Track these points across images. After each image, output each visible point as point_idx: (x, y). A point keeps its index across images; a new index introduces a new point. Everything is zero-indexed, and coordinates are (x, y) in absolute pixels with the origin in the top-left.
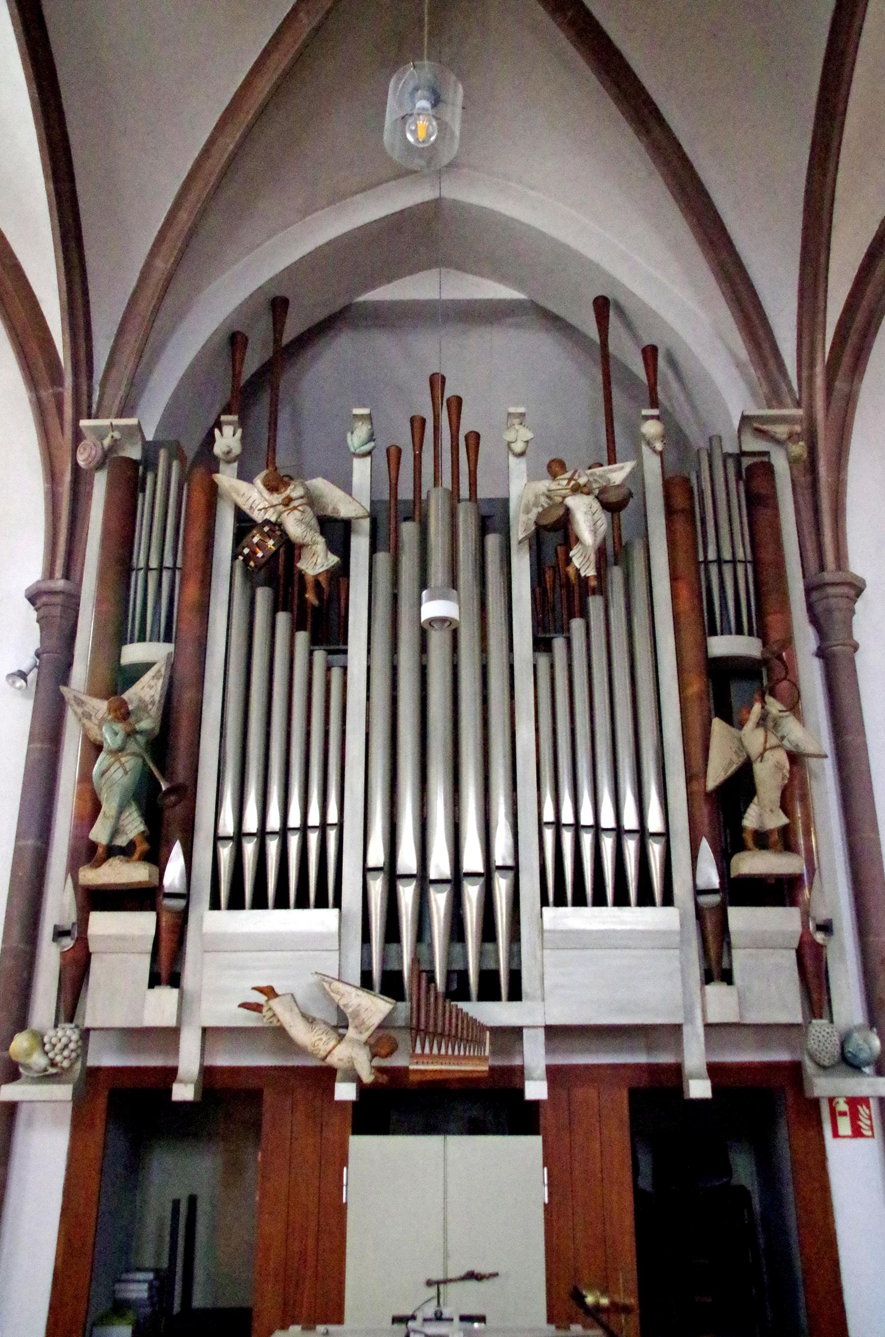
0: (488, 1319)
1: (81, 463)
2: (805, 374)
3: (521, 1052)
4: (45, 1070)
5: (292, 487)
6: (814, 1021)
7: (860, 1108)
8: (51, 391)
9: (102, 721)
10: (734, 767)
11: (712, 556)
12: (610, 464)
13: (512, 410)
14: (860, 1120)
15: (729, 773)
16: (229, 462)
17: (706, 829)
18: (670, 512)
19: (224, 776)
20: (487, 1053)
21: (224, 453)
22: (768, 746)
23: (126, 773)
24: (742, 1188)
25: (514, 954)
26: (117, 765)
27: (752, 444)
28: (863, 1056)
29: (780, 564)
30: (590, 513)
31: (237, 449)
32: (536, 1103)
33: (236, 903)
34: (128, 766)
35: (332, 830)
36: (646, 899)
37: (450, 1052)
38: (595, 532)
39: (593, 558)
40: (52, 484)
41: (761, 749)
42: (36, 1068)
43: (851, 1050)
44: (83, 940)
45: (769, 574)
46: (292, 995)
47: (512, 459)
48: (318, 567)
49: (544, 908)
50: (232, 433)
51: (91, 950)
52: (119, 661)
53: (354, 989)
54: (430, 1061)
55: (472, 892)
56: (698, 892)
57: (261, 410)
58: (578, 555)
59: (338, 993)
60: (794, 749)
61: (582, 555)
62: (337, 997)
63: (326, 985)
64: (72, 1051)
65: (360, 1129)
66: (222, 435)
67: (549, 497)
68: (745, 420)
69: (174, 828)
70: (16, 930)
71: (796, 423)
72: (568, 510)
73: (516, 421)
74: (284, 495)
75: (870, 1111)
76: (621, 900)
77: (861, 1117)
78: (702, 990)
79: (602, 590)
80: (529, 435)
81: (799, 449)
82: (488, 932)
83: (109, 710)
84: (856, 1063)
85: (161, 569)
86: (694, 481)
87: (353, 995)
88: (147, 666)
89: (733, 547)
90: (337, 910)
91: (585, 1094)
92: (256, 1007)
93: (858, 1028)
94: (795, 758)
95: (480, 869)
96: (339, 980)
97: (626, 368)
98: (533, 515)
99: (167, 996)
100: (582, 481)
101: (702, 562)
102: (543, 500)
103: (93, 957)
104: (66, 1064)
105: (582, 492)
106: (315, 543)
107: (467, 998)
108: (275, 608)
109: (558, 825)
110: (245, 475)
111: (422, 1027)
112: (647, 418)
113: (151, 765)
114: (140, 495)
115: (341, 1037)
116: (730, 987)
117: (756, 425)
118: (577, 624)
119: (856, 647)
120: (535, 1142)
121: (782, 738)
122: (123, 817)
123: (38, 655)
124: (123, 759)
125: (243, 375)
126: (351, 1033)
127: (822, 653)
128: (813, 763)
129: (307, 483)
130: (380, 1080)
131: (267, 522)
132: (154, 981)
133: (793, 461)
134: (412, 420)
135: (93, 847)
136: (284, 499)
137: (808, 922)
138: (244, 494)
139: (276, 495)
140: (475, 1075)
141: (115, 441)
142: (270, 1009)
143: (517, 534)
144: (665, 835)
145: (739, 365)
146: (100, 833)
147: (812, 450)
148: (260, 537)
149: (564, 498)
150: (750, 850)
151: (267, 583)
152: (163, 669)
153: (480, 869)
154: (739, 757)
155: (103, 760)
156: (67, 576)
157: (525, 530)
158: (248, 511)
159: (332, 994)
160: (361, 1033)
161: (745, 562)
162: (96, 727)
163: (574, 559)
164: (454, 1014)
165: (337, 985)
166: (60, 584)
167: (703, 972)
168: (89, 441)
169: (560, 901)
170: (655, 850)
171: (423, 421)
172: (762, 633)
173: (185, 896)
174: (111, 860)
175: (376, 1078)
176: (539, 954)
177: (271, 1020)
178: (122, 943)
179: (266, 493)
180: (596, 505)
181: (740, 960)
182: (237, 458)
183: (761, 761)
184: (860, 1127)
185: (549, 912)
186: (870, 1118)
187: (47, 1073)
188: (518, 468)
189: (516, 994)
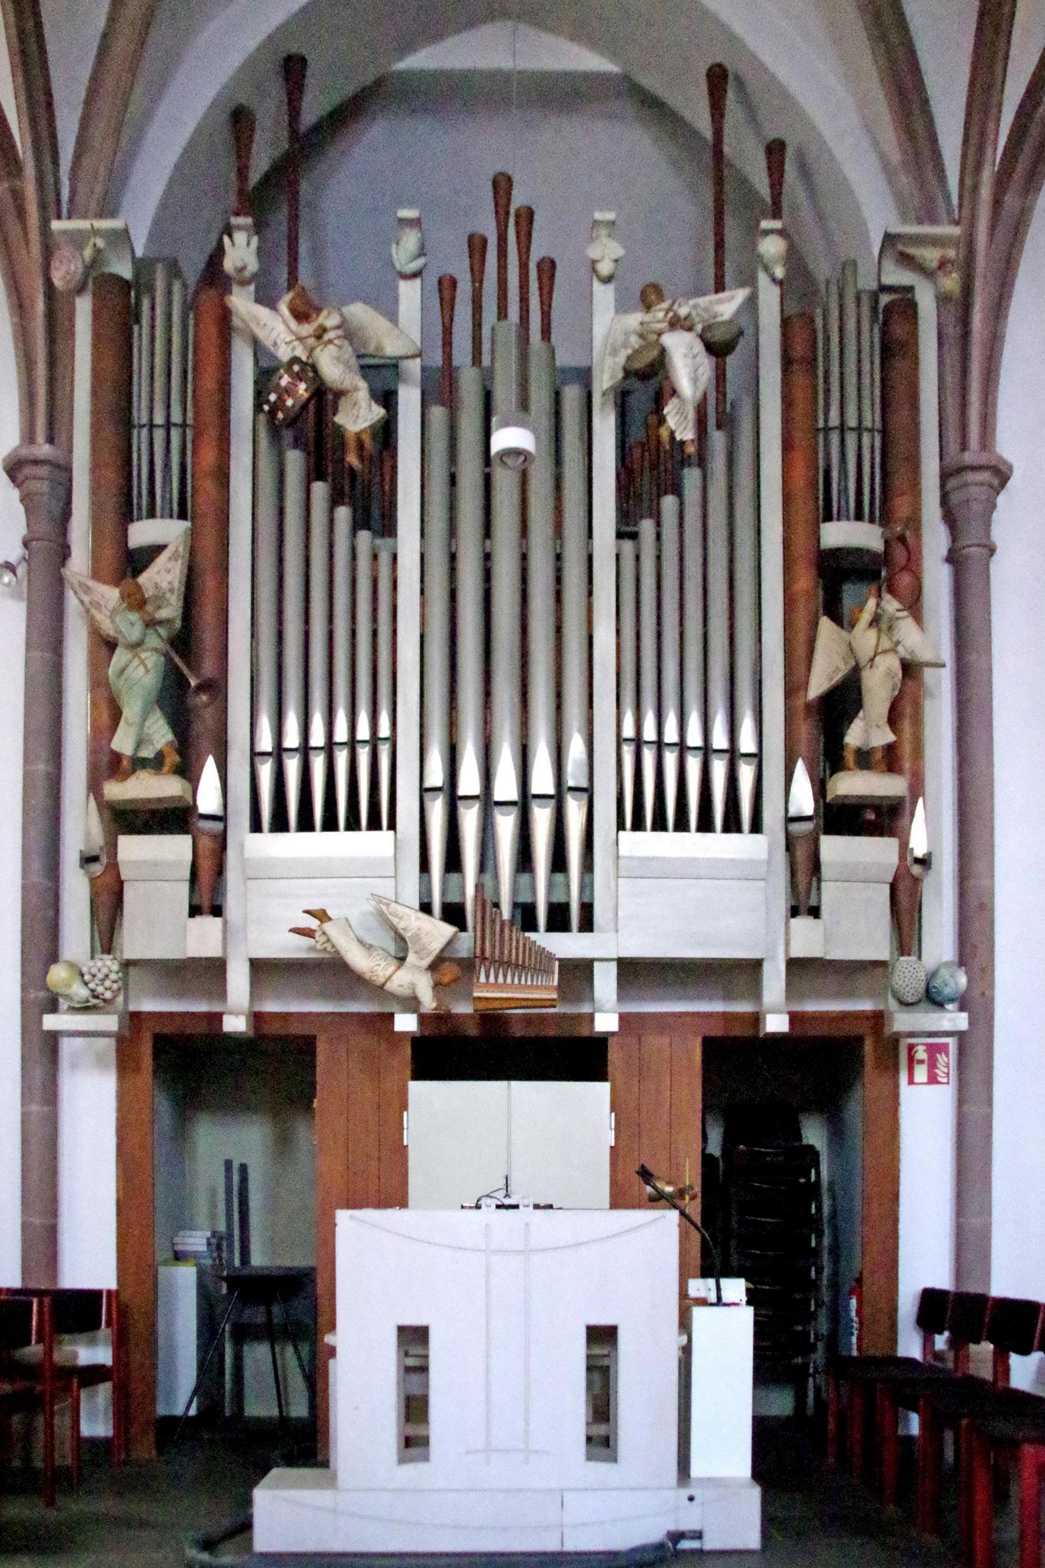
1: (57, 282)
2: (968, 182)
4: (88, 1001)
6: (902, 958)
7: (938, 1056)
8: (6, 185)
9: (114, 612)
11: (834, 420)
12: (717, 291)
13: (598, 216)
14: (937, 1068)
15: (833, 682)
16: (244, 283)
18: (787, 362)
19: (258, 692)
21: (236, 269)
22: (880, 650)
23: (147, 671)
24: (812, 1147)
25: (587, 885)
26: (136, 661)
27: (895, 276)
28: (947, 991)
29: (914, 461)
30: (691, 355)
31: (253, 265)
33: (280, 824)
34: (150, 664)
35: (384, 745)
37: (516, 981)
38: (695, 380)
40: (21, 318)
42: (76, 998)
43: (937, 985)
44: (114, 866)
45: (900, 447)
46: (347, 920)
47: (597, 287)
48: (360, 421)
49: (621, 833)
50: (245, 242)
51: (123, 878)
52: (126, 543)
53: (413, 911)
55: (542, 818)
56: (790, 820)
57: (281, 217)
59: (396, 916)
60: (908, 657)
61: (677, 413)
62: (395, 921)
63: (384, 908)
64: (113, 982)
65: (422, 1073)
67: (641, 336)
68: (890, 239)
69: (205, 743)
70: (37, 865)
72: (663, 351)
73: (603, 232)
74: (315, 324)
75: (948, 1060)
76: (705, 825)
77: (938, 1065)
78: (787, 924)
79: (702, 461)
80: (619, 251)
81: (951, 282)
82: (559, 862)
83: (122, 597)
84: (939, 999)
85: (168, 426)
86: (819, 322)
87: (413, 918)
88: (158, 549)
89: (859, 361)
90: (392, 833)
91: (656, 1042)
92: (307, 933)
93: (947, 965)
94: (910, 669)
95: (551, 791)
96: (396, 902)
97: (744, 181)
98: (621, 359)
99: (210, 925)
100: (683, 311)
103: (126, 885)
104: (108, 995)
105: (682, 328)
107: (534, 928)
109: (638, 742)
110: (266, 298)
112: (767, 233)
113: (177, 660)
114: (136, 328)
116: (816, 920)
117: (900, 247)
118: (669, 503)
119: (992, 550)
120: (601, 1090)
121: (898, 643)
122: (147, 724)
123: (26, 544)
124: (143, 655)
126: (411, 958)
127: (953, 558)
128: (928, 674)
129: (344, 309)
131: (295, 360)
132: (195, 911)
133: (943, 299)
135: (116, 758)
136: (315, 330)
138: (265, 325)
139: (306, 326)
141: (98, 251)
143: (602, 381)
144: (758, 757)
145: (886, 166)
147: (967, 290)
148: (290, 380)
149: (660, 334)
150: (849, 769)
151: (296, 444)
153: (551, 791)
154: (846, 663)
155: (120, 656)
156: (51, 440)
159: (390, 917)
160: (422, 959)
161: (871, 431)
162: (108, 621)
165: (393, 905)
166: (43, 450)
168: (65, 252)
169: (638, 825)
170: (746, 774)
171: (484, 241)
172: (885, 518)
173: (222, 819)
176: (613, 884)
177: (325, 945)
178: (155, 872)
179: (293, 324)
180: (699, 347)
181: (829, 894)
182: (255, 277)
183: (871, 667)
184: (936, 1074)
185: (628, 837)
186: (948, 1066)
187: (89, 1004)
188: (604, 296)
189: (587, 924)
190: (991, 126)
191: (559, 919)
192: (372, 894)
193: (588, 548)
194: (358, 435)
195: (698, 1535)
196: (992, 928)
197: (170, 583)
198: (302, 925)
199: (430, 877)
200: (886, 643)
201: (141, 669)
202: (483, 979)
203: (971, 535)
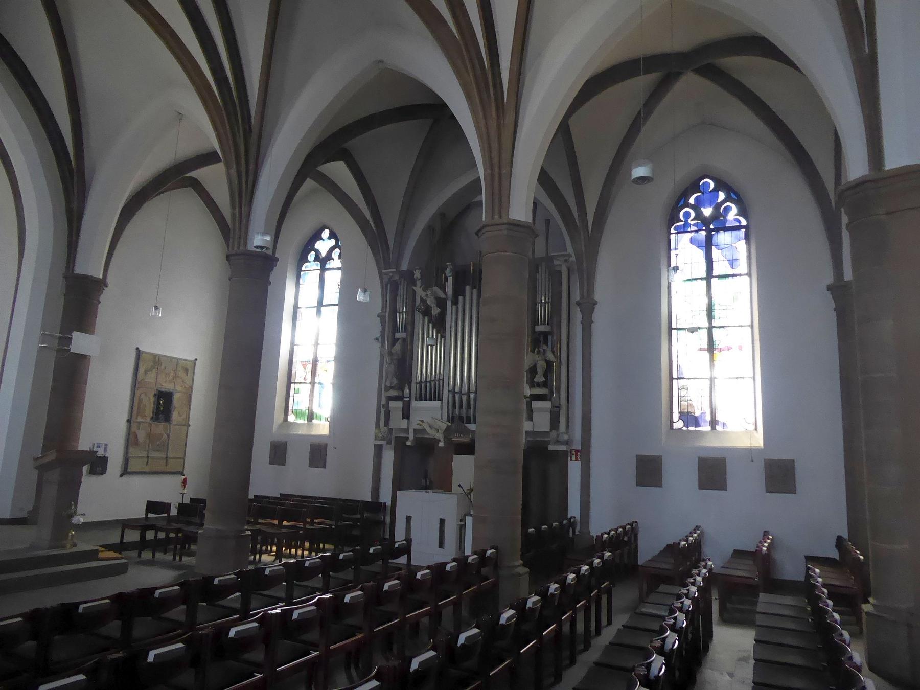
92: (420, 425)
99: (406, 421)
125: (477, 198)
132: (403, 418)
181: (535, 415)
192: (433, 418)
194: (436, 315)
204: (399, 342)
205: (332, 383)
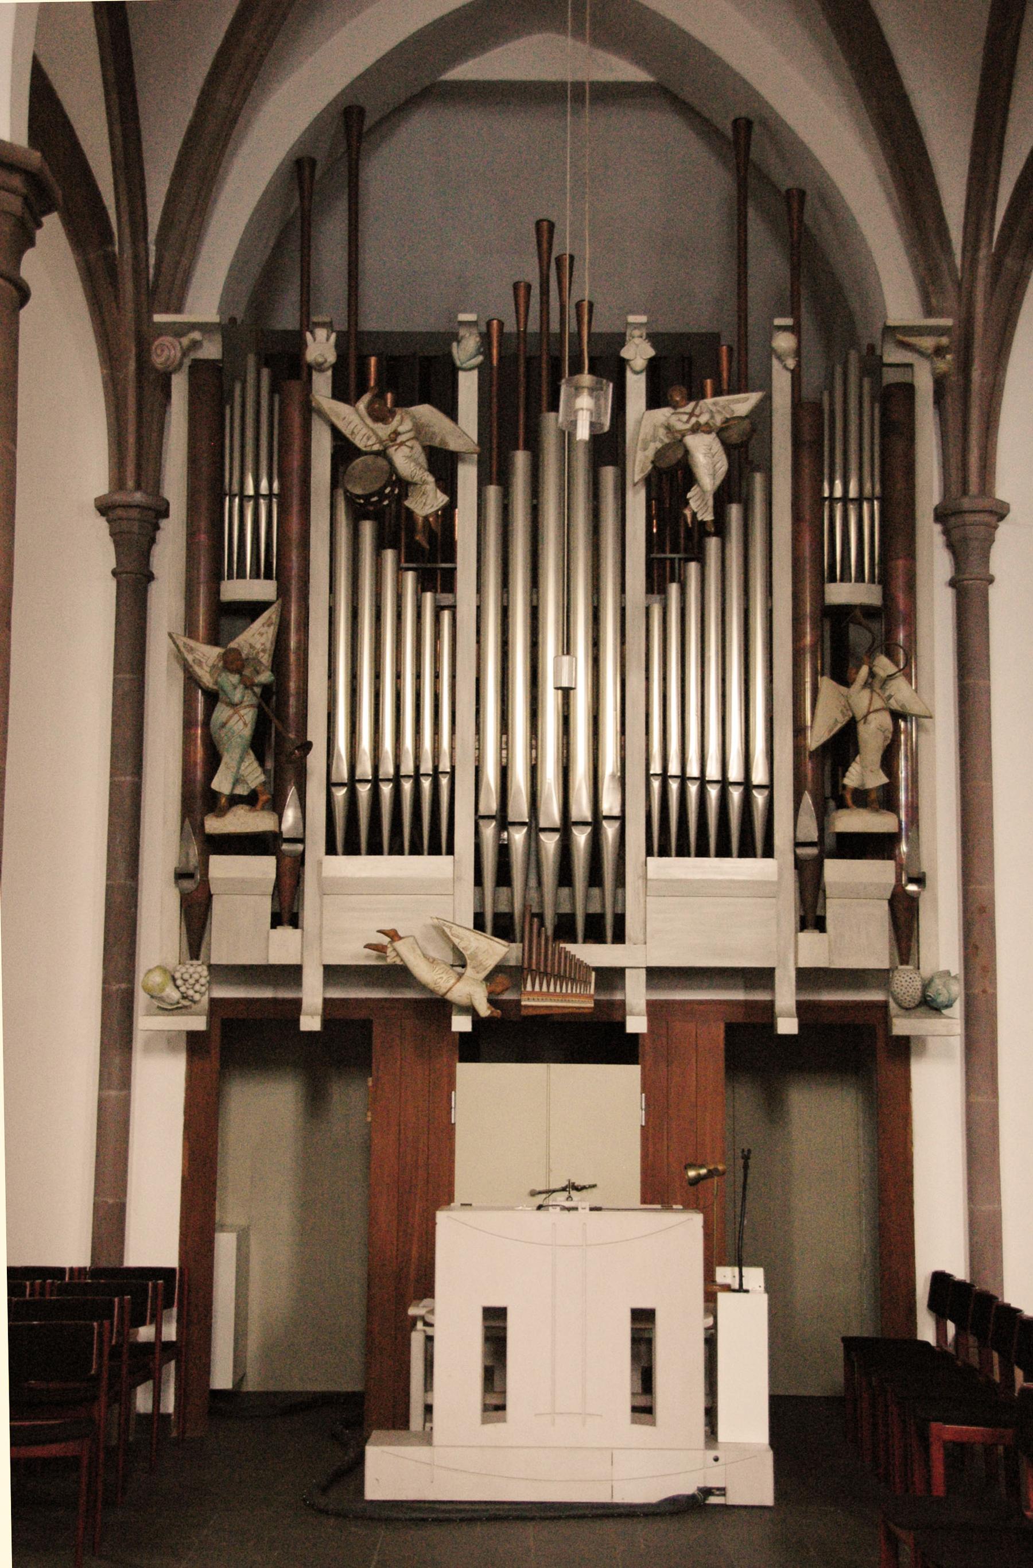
0: (598, 1184)
3: (623, 988)
4: (178, 1003)
5: (398, 418)
10: (839, 726)
11: (838, 493)
17: (810, 785)
20: (592, 991)
22: (871, 710)
23: (245, 724)
25: (619, 900)
26: (236, 718)
32: (636, 1036)
36: (747, 851)
37: (558, 990)
38: (714, 475)
39: (711, 502)
41: (865, 711)
44: (205, 882)
48: (427, 508)
51: (212, 892)
54: (540, 998)
56: (797, 844)
58: (696, 498)
59: (458, 937)
62: (456, 941)
66: (315, 340)
71: (942, 335)
72: (687, 452)
78: (796, 937)
79: (720, 528)
81: (944, 364)
82: (595, 878)
101: (827, 498)
102: (662, 432)
103: (214, 897)
106: (425, 483)
107: (574, 940)
108: (379, 547)
110: (341, 393)
111: (534, 967)
115: (460, 976)
117: (900, 337)
121: (890, 697)
124: (242, 712)
126: (469, 971)
130: (495, 1014)
132: (276, 921)
134: (516, 286)
135: (215, 795)
137: (901, 874)
138: (344, 418)
140: (581, 1011)
142: (395, 950)
144: (770, 787)
146: (222, 783)
152: (274, 617)
157: (642, 471)
158: (348, 436)
159: (451, 937)
160: (478, 973)
163: (691, 501)
164: (563, 957)
167: (798, 919)
169: (664, 852)
171: (529, 287)
174: (234, 809)
175: (492, 1012)
176: (642, 901)
178: (242, 887)
181: (833, 910)
183: (865, 723)
185: (654, 861)
187: (180, 1005)
189: (619, 937)
190: (986, 216)
191: (595, 932)
193: (621, 602)
194: (426, 518)
195: (722, 1491)
196: (434, 1238)
197: (263, 644)
198: (374, 942)
199: (483, 890)
200: (878, 703)
201: (241, 723)
202: (529, 988)
203: (974, 570)
204: (266, 615)
205: (863, 785)
